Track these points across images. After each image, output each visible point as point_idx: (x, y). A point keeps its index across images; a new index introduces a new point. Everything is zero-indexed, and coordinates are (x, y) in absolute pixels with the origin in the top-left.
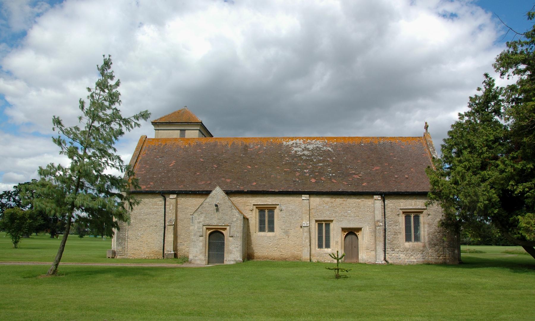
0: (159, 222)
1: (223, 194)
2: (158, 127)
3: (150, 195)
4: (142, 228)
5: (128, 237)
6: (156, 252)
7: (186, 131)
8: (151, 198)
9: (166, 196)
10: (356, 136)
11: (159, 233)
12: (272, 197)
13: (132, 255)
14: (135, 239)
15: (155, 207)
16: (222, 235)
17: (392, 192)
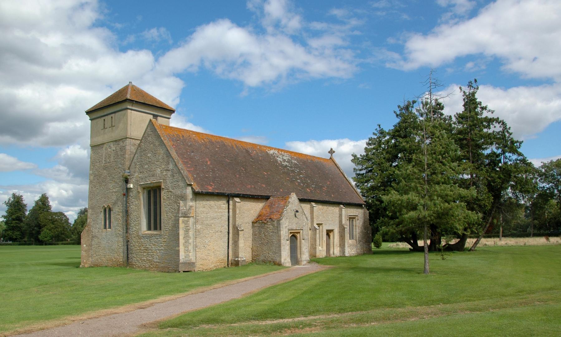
0: (223, 228)
1: (298, 200)
2: (132, 106)
3: (215, 198)
4: (209, 234)
5: (196, 245)
6: (221, 260)
7: (159, 118)
8: (216, 200)
9: (231, 199)
10: (236, 139)
11: (223, 240)
12: (251, 202)
13: (200, 266)
14: (203, 247)
15: (220, 210)
16: (295, 239)
17: (358, 204)
